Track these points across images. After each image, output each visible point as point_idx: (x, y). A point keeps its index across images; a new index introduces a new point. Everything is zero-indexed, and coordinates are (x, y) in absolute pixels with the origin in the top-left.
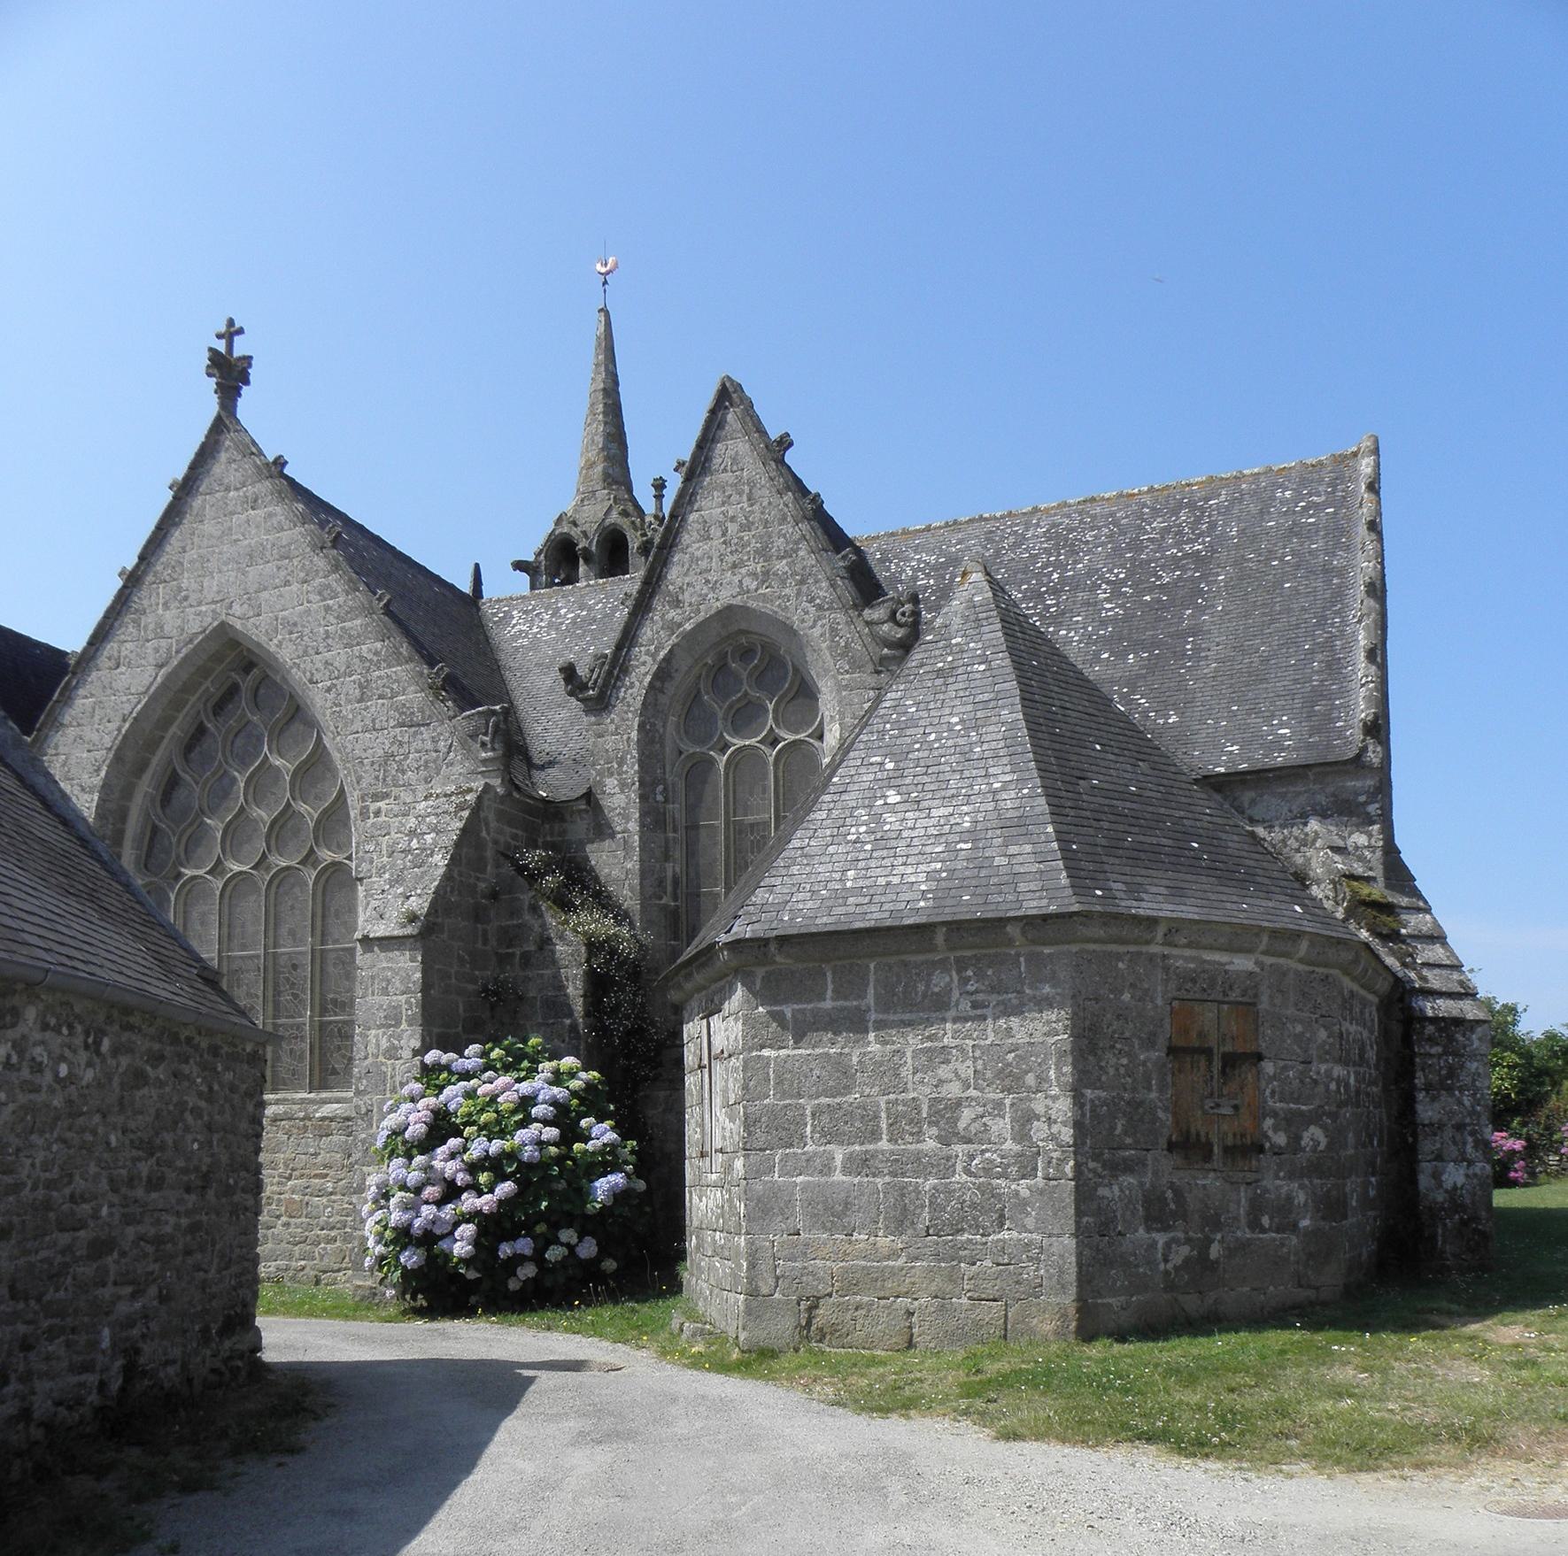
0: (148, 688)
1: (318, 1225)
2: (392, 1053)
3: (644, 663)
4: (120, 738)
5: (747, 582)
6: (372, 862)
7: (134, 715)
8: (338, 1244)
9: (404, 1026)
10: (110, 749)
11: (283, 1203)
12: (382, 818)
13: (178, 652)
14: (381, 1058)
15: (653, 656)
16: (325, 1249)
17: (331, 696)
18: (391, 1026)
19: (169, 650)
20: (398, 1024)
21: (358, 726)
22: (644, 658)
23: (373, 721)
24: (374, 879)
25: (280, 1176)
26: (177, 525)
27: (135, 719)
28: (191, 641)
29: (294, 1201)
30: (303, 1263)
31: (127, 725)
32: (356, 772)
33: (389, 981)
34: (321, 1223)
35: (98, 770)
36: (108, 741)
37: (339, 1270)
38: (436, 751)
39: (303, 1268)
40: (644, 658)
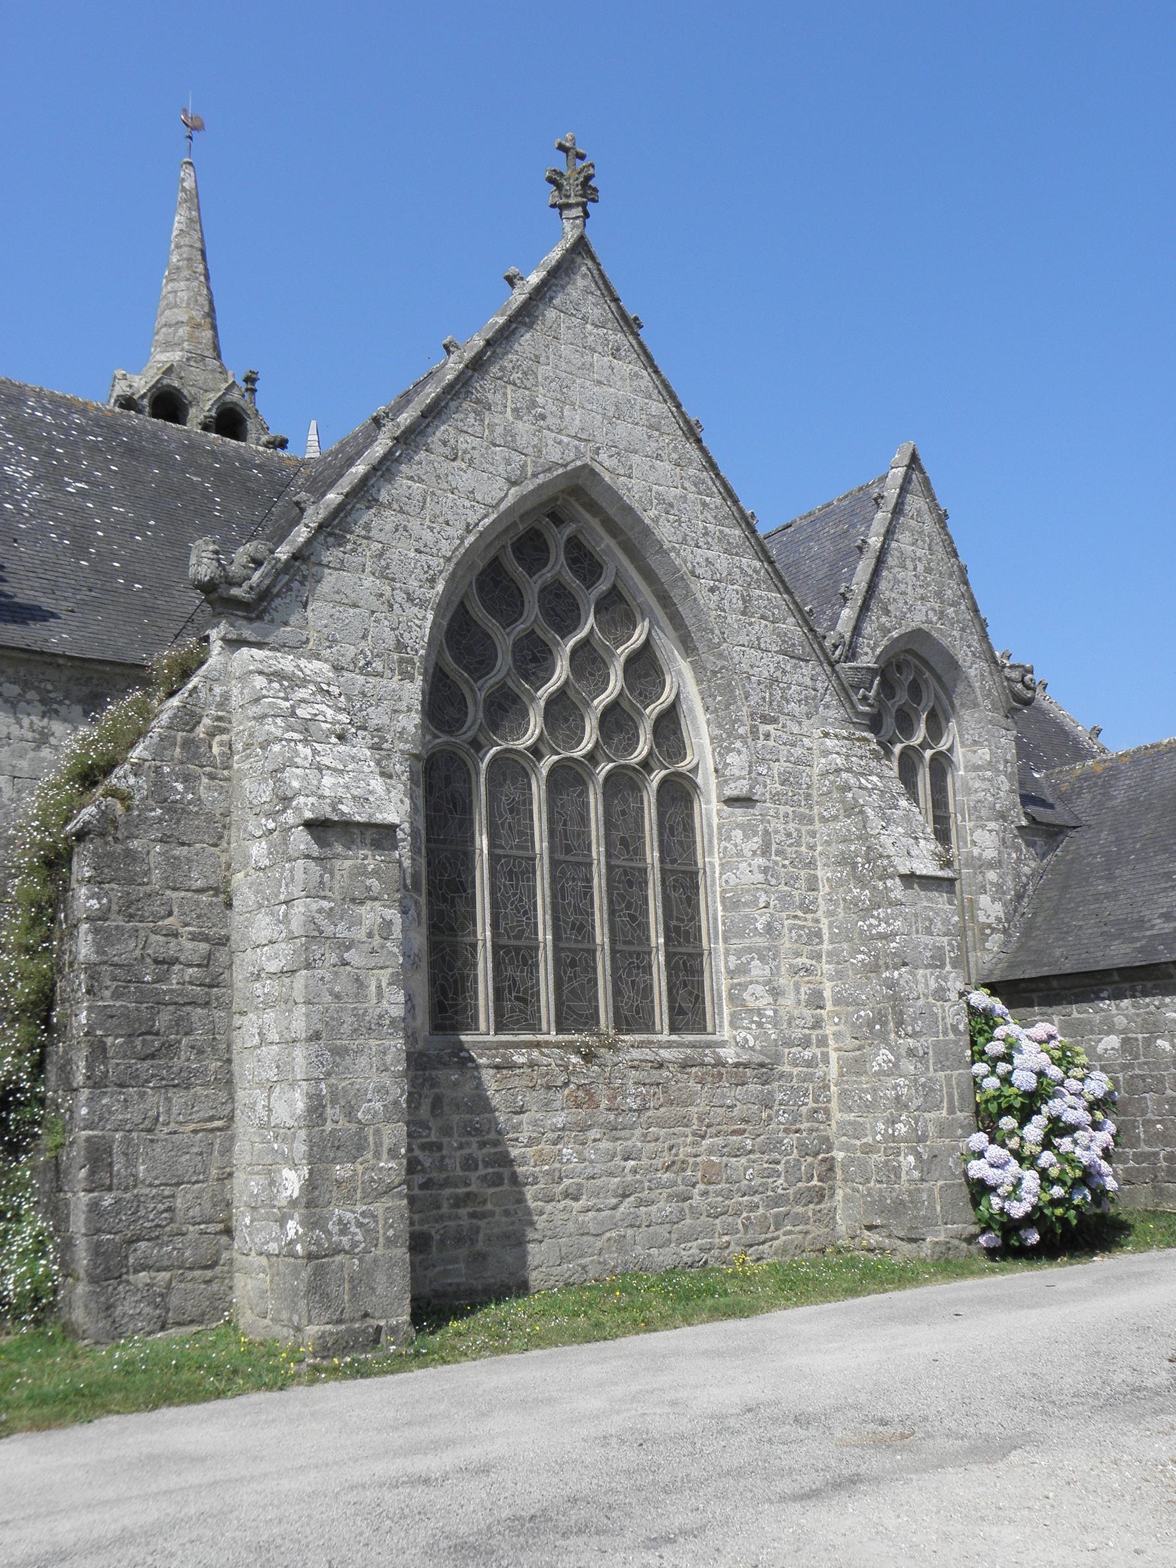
0: (498, 504)
1: (739, 1190)
2: (940, 994)
3: (866, 654)
4: (462, 550)
5: (931, 614)
6: (765, 786)
7: (480, 528)
8: (761, 1211)
9: (948, 968)
10: (449, 560)
11: (700, 1167)
12: (771, 743)
13: (535, 475)
14: (931, 1000)
15: (873, 649)
16: (748, 1218)
17: (715, 597)
18: (938, 967)
19: (524, 467)
20: (943, 966)
21: (743, 639)
22: (866, 649)
23: (758, 639)
24: (768, 805)
25: (694, 1134)
26: (530, 326)
27: (481, 533)
28: (549, 470)
29: (713, 1164)
30: (725, 1238)
31: (471, 539)
32: (744, 687)
33: (931, 921)
34: (744, 1188)
35: (432, 581)
36: (446, 548)
37: (763, 1243)
38: (815, 690)
39: (729, 1243)
40: (866, 649)
